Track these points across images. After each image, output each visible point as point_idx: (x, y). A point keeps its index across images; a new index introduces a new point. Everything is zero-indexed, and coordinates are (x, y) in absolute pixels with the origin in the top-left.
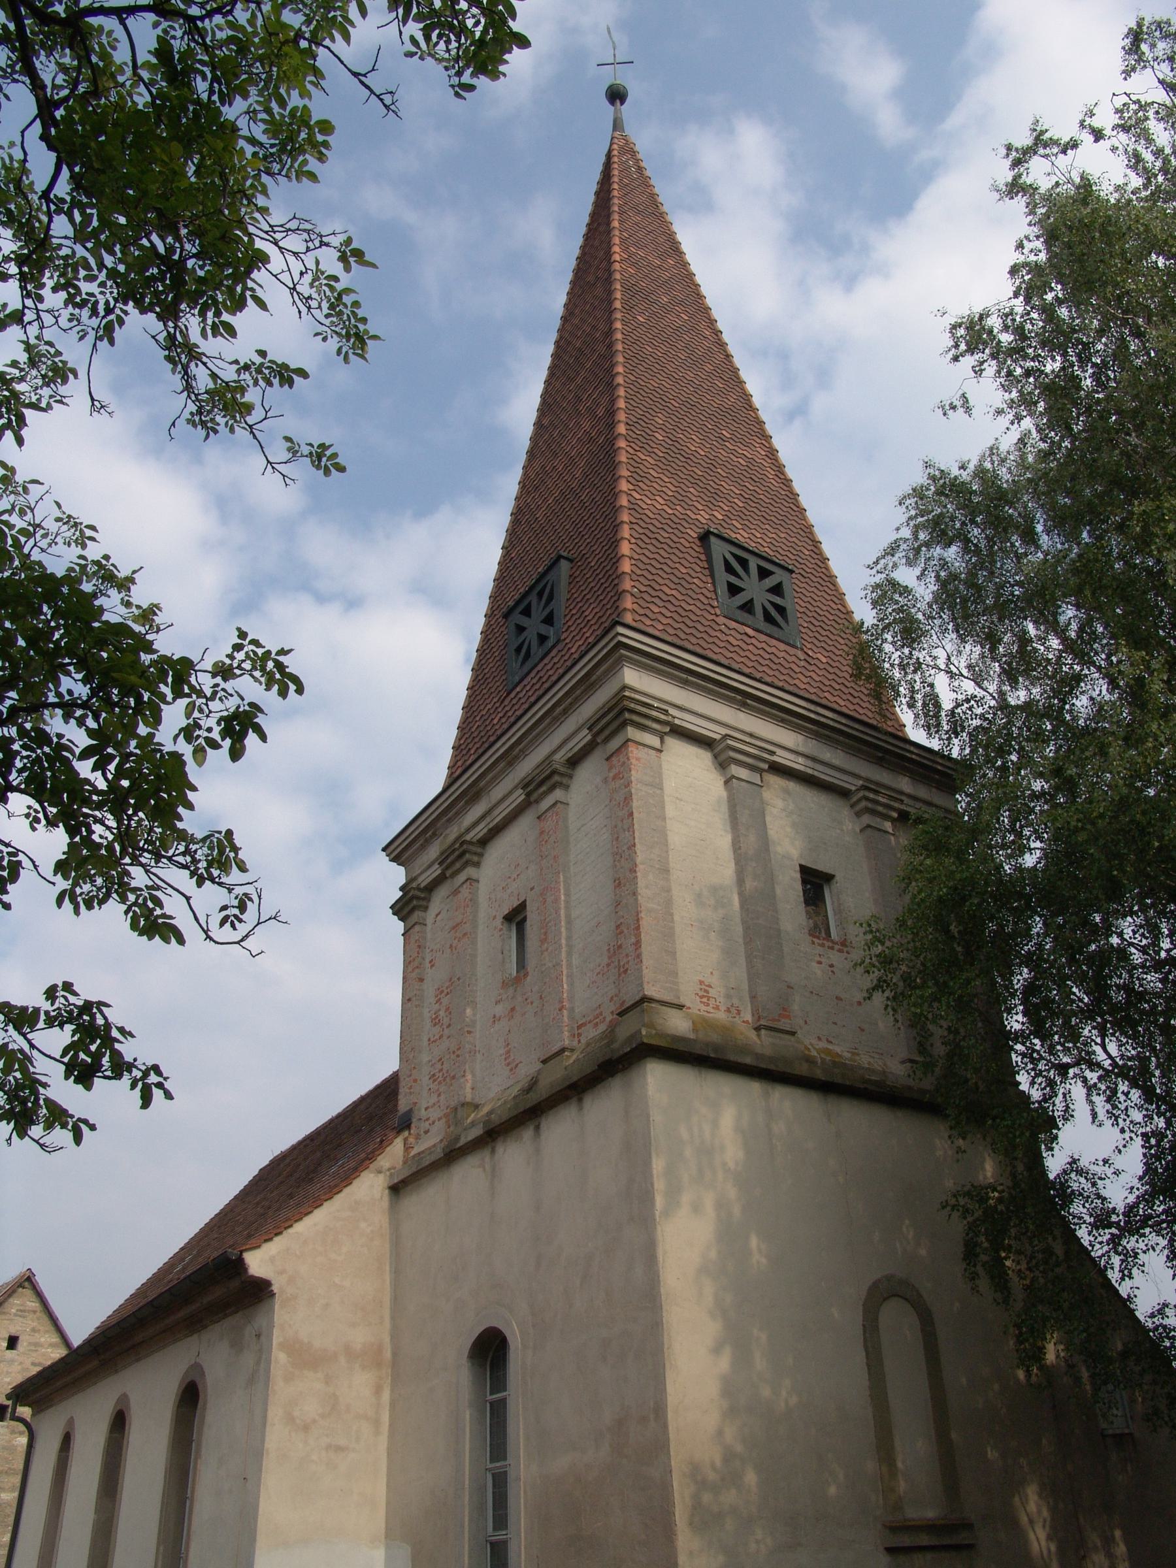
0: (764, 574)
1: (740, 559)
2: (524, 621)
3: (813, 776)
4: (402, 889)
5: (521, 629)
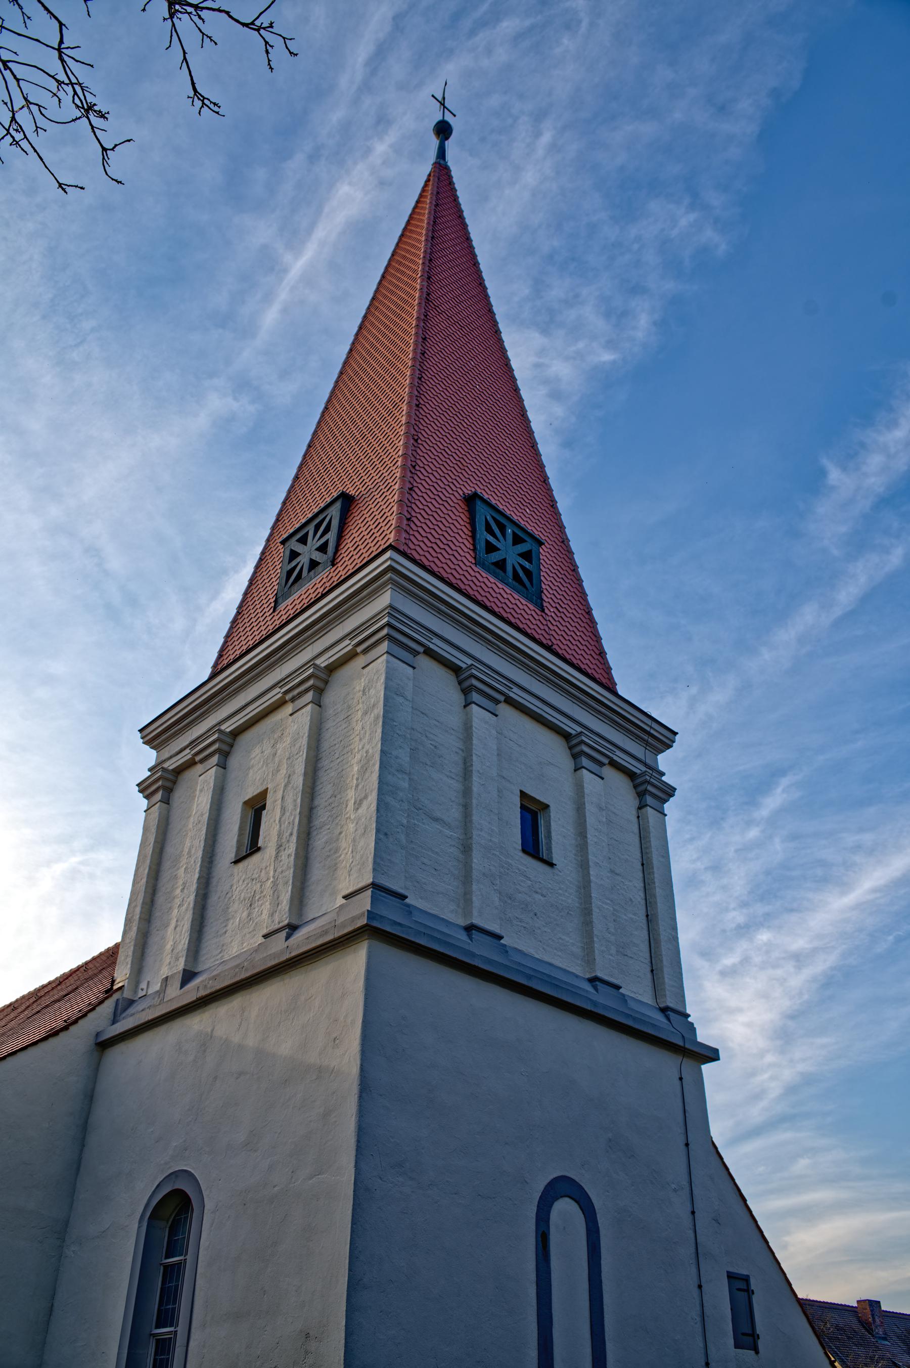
0: (517, 540)
1: (502, 521)
2: (299, 548)
3: (541, 715)
4: (150, 770)
5: (294, 555)
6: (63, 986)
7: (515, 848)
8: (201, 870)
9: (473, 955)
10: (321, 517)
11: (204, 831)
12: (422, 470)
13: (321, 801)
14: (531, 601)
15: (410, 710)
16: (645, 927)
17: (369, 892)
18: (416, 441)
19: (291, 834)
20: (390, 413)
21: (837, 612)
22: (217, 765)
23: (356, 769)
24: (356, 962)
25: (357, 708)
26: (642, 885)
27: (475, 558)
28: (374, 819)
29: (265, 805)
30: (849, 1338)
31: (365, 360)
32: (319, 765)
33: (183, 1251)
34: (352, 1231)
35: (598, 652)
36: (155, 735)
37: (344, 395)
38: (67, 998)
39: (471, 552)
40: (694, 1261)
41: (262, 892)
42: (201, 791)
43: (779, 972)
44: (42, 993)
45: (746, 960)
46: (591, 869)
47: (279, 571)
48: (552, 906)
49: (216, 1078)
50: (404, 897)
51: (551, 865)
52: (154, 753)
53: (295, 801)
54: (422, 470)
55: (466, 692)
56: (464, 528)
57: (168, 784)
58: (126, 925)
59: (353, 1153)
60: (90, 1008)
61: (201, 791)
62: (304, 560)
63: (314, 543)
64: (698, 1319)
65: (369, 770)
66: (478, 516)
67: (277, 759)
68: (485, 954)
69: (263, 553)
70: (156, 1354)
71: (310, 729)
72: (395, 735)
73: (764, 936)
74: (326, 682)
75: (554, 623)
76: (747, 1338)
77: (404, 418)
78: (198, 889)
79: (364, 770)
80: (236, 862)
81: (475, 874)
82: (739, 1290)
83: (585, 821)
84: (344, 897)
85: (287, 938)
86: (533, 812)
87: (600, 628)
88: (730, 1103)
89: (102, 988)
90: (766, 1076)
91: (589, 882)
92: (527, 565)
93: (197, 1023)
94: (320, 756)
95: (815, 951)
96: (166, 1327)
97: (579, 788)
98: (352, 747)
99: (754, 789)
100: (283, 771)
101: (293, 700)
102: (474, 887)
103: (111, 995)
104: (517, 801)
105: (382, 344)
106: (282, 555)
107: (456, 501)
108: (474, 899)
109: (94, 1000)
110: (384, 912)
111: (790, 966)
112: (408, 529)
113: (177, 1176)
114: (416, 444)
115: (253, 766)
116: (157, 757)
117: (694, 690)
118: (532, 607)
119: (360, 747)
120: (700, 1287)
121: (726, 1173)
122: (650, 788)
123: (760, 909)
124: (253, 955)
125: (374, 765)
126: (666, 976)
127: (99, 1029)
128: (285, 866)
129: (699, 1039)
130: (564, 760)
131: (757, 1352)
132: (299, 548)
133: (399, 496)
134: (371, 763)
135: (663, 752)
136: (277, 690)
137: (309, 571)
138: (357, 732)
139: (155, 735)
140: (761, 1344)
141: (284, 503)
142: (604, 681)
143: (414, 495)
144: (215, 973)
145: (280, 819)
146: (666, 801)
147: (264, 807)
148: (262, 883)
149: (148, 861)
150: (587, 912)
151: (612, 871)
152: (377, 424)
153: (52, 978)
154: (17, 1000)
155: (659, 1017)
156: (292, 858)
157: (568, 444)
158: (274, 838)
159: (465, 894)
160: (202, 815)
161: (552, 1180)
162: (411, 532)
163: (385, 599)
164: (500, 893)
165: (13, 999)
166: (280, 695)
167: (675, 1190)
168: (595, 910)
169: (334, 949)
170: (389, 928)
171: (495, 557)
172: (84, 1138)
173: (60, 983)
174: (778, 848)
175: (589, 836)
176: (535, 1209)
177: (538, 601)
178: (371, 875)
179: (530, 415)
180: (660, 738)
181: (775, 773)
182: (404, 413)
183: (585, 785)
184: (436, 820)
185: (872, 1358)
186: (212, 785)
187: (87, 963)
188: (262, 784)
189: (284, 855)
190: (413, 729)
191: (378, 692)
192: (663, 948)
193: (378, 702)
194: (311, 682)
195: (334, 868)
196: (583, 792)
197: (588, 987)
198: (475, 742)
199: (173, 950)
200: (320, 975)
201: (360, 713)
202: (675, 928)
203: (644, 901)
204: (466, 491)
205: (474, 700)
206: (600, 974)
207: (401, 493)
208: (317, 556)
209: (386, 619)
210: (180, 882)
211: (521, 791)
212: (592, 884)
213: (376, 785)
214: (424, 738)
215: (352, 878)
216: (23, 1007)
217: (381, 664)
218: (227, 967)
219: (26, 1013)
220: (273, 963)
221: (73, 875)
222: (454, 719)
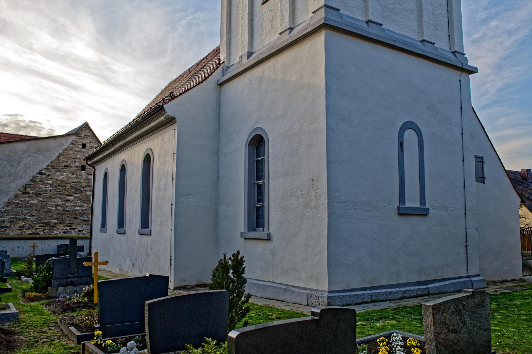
6: (199, 65)
8: (249, 9)
9: (370, 33)
16: (447, 16)
17: (323, 9)
24: (320, 40)
34: (327, 144)
40: (462, 151)
45: (485, 35)
49: (267, 92)
50: (339, 10)
70: (258, 189)
73: (494, 23)
76: (481, 178)
78: (249, 18)
80: (263, 4)
89: (215, 63)
102: (369, 3)
109: (213, 68)
126: (455, 38)
129: (469, 64)
131: (484, 183)
140: (486, 181)
148: (276, 11)
150: (420, 10)
155: (452, 56)
159: (365, 7)
167: (455, 125)
168: (424, 10)
176: (398, 134)
197: (420, 44)
203: (446, 5)
210: (241, 16)
220: (286, 43)
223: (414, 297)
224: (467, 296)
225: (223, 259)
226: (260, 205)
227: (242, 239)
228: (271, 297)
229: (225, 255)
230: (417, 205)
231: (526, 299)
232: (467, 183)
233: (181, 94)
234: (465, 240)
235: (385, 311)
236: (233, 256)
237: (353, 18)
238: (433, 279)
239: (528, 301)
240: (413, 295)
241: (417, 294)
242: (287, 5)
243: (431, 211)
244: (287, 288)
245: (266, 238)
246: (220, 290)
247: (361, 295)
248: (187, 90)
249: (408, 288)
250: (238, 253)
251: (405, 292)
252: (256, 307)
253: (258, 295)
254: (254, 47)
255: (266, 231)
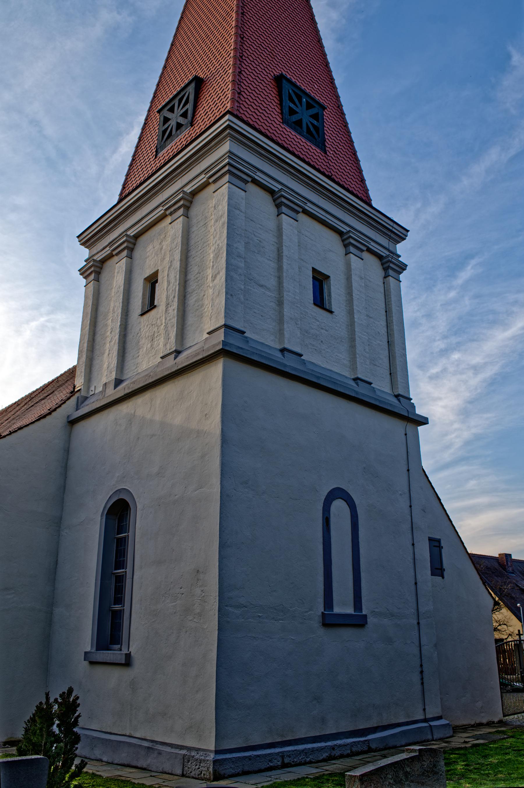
0: (309, 106)
1: (299, 93)
2: (169, 115)
4: (86, 261)
6: (45, 391)
7: (309, 303)
8: (121, 321)
9: (285, 366)
10: (182, 94)
11: (121, 297)
12: (247, 59)
13: (191, 276)
14: (318, 146)
15: (244, 218)
16: (387, 349)
17: (223, 330)
18: (242, 39)
19: (174, 297)
20: (224, 19)
21: (512, 152)
22: (126, 256)
23: (212, 256)
24: (216, 370)
25: (211, 218)
26: (386, 324)
27: (282, 119)
28: (224, 286)
29: (157, 280)
30: (493, 573)
31: (196, 11)
32: (189, 255)
33: (127, 530)
34: (220, 518)
35: (360, 180)
36: (88, 239)
37: (193, 8)
38: (48, 397)
39: (279, 115)
40: (410, 531)
41: (159, 332)
42: (118, 273)
43: (464, 377)
44: (33, 396)
45: (444, 370)
46: (355, 315)
47: (157, 131)
48: (332, 336)
49: (138, 438)
50: (243, 333)
51: (331, 312)
52: (87, 250)
53: (175, 277)
54: (247, 59)
55: (278, 206)
56: (275, 99)
57: (98, 269)
58: (79, 354)
59: (219, 476)
60: (61, 404)
61: (118, 273)
62: (173, 123)
63: (178, 111)
64: (412, 561)
65: (220, 256)
66: (284, 90)
67: (163, 252)
68: (292, 365)
69: (146, 119)
71: (183, 232)
72: (235, 234)
73: (456, 356)
74: (191, 202)
75: (333, 161)
76: (438, 570)
77: (234, 22)
79: (217, 256)
80: (142, 315)
81: (286, 318)
82: (435, 546)
83: (352, 286)
84: (208, 333)
85: (175, 358)
86: (320, 280)
87: (362, 164)
88: (434, 448)
89: (68, 391)
90: (453, 436)
91: (354, 322)
92: (315, 122)
93: (125, 408)
94: (190, 249)
95: (486, 364)
96: (120, 569)
97: (348, 265)
98: (209, 242)
99: (454, 267)
100: (167, 259)
101: (171, 214)
102: (285, 326)
103: (74, 395)
104: (310, 273)
105: (203, 12)
106: (158, 120)
107: (269, 80)
108: (285, 333)
109: (64, 398)
110: (231, 341)
111: (470, 373)
112: (239, 100)
113: (120, 492)
114: (242, 41)
115: (148, 257)
116: (90, 253)
117: (419, 205)
118: (319, 151)
119: (214, 242)
120: (413, 545)
121: (430, 485)
122: (391, 265)
123: (454, 340)
124: (156, 369)
125: (223, 253)
126: (398, 377)
127: (70, 414)
128: (172, 317)
130: (340, 249)
131: (443, 578)
132: (169, 115)
133: (232, 78)
134: (221, 252)
135: (400, 242)
136: (161, 208)
137: (177, 130)
138: (211, 234)
139: (88, 239)
140: (445, 574)
141: (158, 85)
142: (364, 198)
143: (242, 76)
144: (134, 380)
145: (167, 288)
146: (400, 273)
147: (157, 281)
148: (159, 327)
149: (89, 316)
150: (352, 339)
151: (368, 316)
152: (216, 28)
153: (38, 387)
154: (19, 400)
155: (395, 400)
156: (176, 311)
157: (340, 40)
158: (164, 300)
160: (119, 287)
161: (333, 489)
162: (241, 102)
163: (226, 147)
164: (301, 329)
165: (17, 400)
166: (163, 211)
167: (401, 495)
168: (357, 338)
169: (204, 363)
170: (234, 351)
171: (295, 118)
172: (66, 473)
173: (43, 390)
174: (467, 303)
175: (354, 295)
177: (322, 145)
178: (224, 320)
179: (317, 19)
180: (398, 234)
181: (468, 256)
182: (234, 19)
183: (352, 264)
184: (262, 286)
185: (505, 583)
186: (124, 269)
187: (57, 378)
188: (155, 267)
189: (170, 310)
190: (246, 230)
191: (224, 207)
192: (397, 361)
193: (224, 213)
194: (181, 203)
195: (201, 316)
196: (351, 268)
197: (353, 383)
198: (284, 237)
199: (108, 368)
200: (195, 379)
201: (213, 221)
202: (405, 349)
203: (386, 334)
204: (275, 73)
205: (283, 211)
206: (360, 376)
207: (234, 75)
208: (181, 120)
209: (227, 160)
210: (110, 328)
211: (313, 268)
212: (356, 324)
213: (225, 266)
214: (253, 236)
215: (212, 322)
216: (23, 404)
217: (225, 190)
218: (140, 376)
219: (25, 406)
220: (169, 372)
221: (42, 329)
222: (271, 224)
223: (348, 756)
224: (411, 758)
225: (44, 701)
226: (117, 607)
227: (86, 663)
228: (126, 763)
229: (47, 695)
230: (350, 610)
231: (507, 754)
232: (419, 577)
233: (10, 433)
234: (419, 664)
235: (302, 781)
236: (61, 696)
237: (262, 343)
238: (375, 725)
239: (508, 757)
240: (345, 753)
241: (351, 752)
242: (175, 320)
243: (371, 620)
244: (152, 747)
245: (123, 662)
246: (34, 757)
247: (266, 755)
248: (20, 428)
249: (339, 742)
250: (70, 691)
251: (333, 749)
252: (99, 780)
253: (105, 759)
254: (126, 372)
255: (125, 651)
